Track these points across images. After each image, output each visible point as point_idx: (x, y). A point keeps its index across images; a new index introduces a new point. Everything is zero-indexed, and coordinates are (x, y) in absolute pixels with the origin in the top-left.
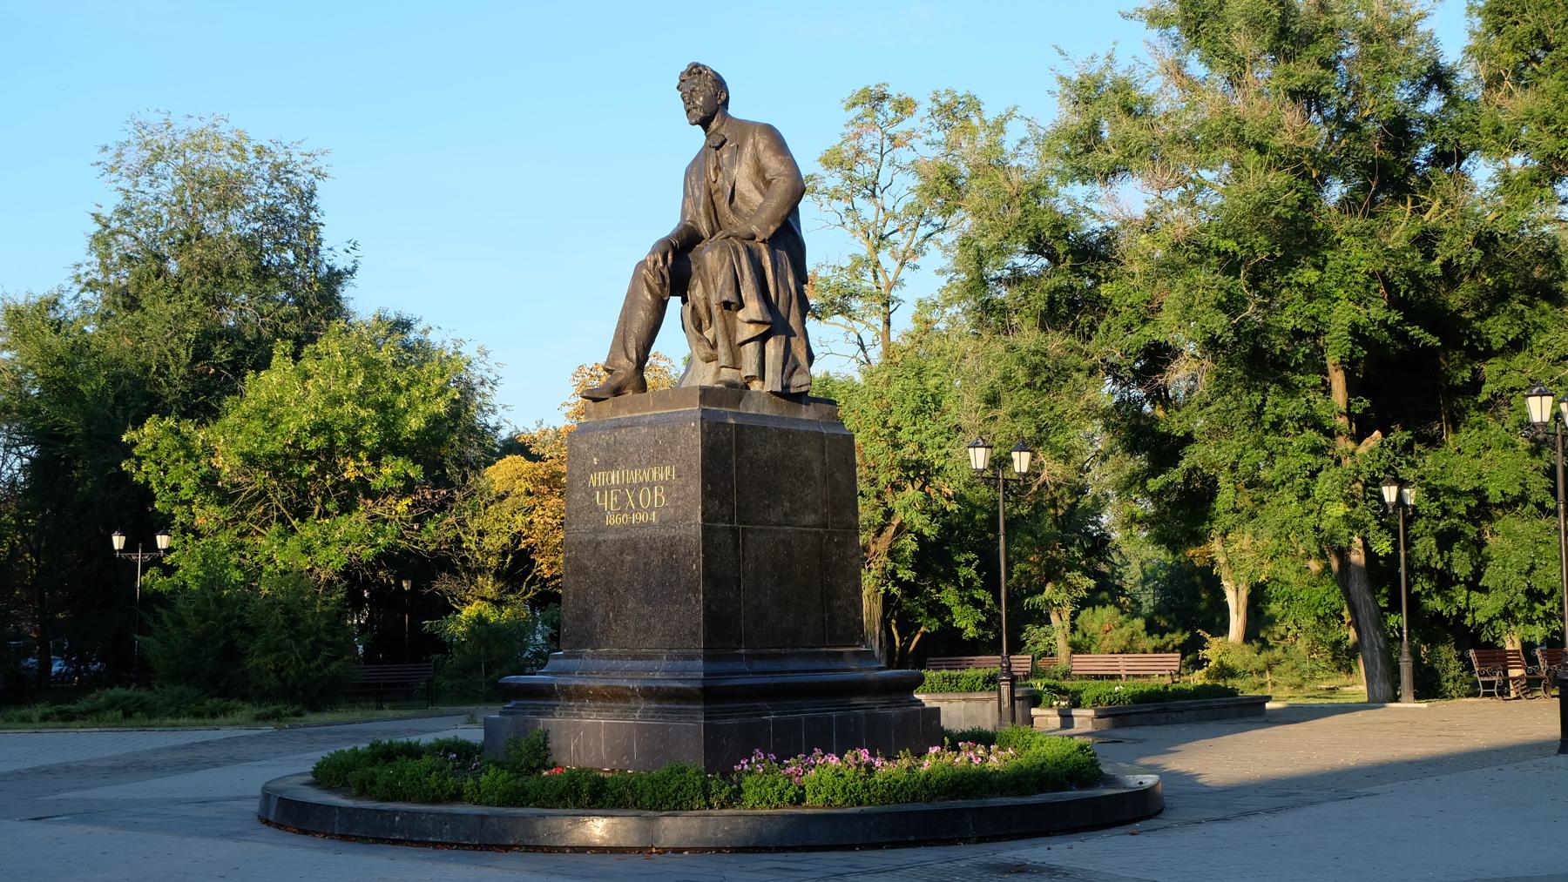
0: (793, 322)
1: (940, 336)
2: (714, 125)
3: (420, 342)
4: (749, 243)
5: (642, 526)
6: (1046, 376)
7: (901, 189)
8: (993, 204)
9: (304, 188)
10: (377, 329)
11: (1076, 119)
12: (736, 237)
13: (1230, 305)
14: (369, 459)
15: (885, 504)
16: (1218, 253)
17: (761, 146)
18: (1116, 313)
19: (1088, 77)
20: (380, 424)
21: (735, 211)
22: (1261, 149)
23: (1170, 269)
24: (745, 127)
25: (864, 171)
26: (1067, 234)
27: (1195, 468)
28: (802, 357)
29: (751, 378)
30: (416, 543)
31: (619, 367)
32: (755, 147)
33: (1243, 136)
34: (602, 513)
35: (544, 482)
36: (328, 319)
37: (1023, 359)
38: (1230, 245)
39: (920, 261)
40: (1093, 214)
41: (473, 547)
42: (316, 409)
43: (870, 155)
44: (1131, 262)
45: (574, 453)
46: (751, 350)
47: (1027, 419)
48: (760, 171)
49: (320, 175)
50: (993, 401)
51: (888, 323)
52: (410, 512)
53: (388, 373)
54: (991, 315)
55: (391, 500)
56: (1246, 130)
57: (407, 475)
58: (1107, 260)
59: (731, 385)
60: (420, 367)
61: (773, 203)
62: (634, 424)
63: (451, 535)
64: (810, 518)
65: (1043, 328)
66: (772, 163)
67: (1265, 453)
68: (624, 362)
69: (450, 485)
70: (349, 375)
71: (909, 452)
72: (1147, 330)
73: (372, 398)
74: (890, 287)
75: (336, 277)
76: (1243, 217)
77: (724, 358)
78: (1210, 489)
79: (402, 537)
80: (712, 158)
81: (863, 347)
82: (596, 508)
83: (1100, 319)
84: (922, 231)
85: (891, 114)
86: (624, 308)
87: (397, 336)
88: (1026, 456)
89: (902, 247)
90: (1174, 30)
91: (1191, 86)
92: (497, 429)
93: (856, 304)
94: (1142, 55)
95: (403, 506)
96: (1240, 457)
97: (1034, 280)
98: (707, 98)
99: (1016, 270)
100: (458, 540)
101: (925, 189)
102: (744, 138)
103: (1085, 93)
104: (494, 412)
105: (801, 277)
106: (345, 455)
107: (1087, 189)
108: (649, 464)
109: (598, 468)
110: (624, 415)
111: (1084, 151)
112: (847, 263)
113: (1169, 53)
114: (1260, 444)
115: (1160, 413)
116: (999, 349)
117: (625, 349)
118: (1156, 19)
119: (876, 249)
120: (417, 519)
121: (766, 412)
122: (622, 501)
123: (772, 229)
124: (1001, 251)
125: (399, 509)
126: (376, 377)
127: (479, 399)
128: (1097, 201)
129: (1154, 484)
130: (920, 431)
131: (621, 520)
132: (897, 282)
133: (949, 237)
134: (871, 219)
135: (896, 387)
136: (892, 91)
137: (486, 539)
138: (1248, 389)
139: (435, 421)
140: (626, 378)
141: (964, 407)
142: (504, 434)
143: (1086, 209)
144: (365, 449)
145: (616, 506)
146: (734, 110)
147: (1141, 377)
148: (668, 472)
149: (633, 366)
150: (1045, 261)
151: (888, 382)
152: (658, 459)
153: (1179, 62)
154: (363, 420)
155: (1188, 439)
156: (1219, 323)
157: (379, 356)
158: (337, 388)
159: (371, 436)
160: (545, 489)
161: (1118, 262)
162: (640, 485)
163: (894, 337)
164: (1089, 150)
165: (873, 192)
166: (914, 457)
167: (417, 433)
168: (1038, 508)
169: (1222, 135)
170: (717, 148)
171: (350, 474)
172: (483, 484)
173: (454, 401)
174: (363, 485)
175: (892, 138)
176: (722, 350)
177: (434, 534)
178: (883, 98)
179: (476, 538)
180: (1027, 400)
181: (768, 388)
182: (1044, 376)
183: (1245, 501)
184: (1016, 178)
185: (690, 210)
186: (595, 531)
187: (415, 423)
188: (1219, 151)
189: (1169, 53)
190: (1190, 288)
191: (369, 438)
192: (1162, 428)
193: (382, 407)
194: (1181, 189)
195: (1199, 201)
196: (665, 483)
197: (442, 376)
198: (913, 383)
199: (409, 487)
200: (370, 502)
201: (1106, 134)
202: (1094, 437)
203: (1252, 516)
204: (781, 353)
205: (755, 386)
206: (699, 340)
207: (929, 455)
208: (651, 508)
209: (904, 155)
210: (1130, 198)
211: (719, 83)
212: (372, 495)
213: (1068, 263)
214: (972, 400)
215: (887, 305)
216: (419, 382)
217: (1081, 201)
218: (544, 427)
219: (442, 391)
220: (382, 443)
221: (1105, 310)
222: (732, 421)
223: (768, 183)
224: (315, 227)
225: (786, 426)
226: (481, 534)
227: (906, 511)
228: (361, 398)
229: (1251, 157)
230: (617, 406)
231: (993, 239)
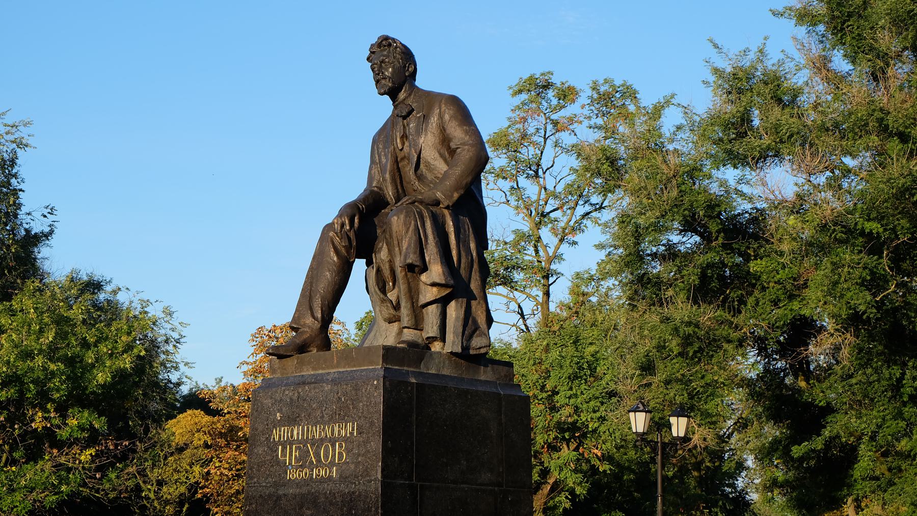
0: (474, 286)
1: (592, 309)
2: (402, 95)
3: (108, 301)
4: (434, 209)
5: (322, 481)
6: (699, 346)
7: (562, 168)
8: (651, 185)
9: (6, 156)
10: (70, 289)
11: (729, 108)
12: (421, 202)
13: (874, 283)
14: (56, 410)
15: (542, 463)
16: (862, 233)
17: (447, 117)
18: (764, 289)
19: (741, 69)
20: (68, 378)
21: (420, 178)
22: (904, 138)
23: (816, 248)
24: (431, 98)
25: (528, 152)
26: (720, 213)
27: (838, 436)
28: (481, 320)
29: (432, 339)
30: (97, 491)
31: (304, 325)
32: (441, 117)
33: (887, 126)
34: (283, 467)
35: (221, 435)
36: (24, 278)
37: (676, 329)
38: (873, 226)
39: (578, 237)
40: (742, 195)
41: (152, 496)
42: (8, 362)
43: (535, 138)
44: (780, 240)
45: (258, 409)
46: (432, 312)
47: (678, 386)
48: (445, 140)
49: (21, 144)
50: (648, 368)
51: (547, 294)
52: (93, 461)
53: (78, 329)
54: (645, 289)
55: (76, 449)
56: (890, 120)
57: (91, 425)
58: (756, 237)
59: (412, 345)
60: (109, 325)
61: (458, 171)
62: (318, 381)
63: (130, 483)
64: (486, 477)
65: (695, 302)
66: (457, 133)
67: (903, 424)
68: (309, 320)
69: (132, 436)
70: (41, 331)
71: (565, 414)
72: (795, 305)
73: (62, 352)
74: (550, 260)
75: (33, 240)
76: (886, 201)
77: (406, 320)
78: (850, 455)
79: (85, 485)
80: (399, 127)
81: (522, 315)
82: (278, 462)
83: (750, 294)
84: (581, 210)
85: (555, 102)
86: (311, 269)
87: (88, 296)
88: (683, 421)
89: (562, 224)
90: (821, 28)
91: (836, 81)
92: (178, 384)
93: (518, 276)
94: (788, 47)
95: (86, 456)
96: (879, 427)
97: (688, 256)
98: (394, 67)
99: (670, 246)
100: (138, 489)
101: (587, 169)
102: (430, 109)
103: (737, 83)
104: (176, 368)
105: (482, 243)
106: (34, 407)
107: (738, 172)
108: (332, 420)
109: (281, 423)
110: (308, 372)
111: (735, 138)
112: (510, 238)
113: (816, 50)
114: (899, 415)
115: (803, 384)
116: (655, 319)
117: (311, 309)
118: (804, 17)
119: (538, 225)
120: (99, 469)
121: (446, 372)
122: (304, 455)
123: (456, 196)
124: (659, 228)
125: (83, 458)
126: (67, 333)
127: (163, 356)
128: (748, 183)
129: (797, 451)
130: (576, 396)
131: (304, 474)
132: (557, 257)
133: (606, 216)
134: (534, 198)
135: (554, 354)
136: (556, 80)
137: (165, 489)
138: (889, 363)
139: (120, 376)
140: (308, 337)
141: (620, 372)
142: (185, 390)
143: (737, 191)
144: (53, 401)
145: (297, 460)
146: (423, 81)
147: (783, 350)
148: (349, 429)
149: (317, 325)
150: (697, 239)
151: (547, 349)
152: (340, 416)
153: (825, 58)
154: (53, 373)
155: (829, 409)
156: (862, 300)
157: (71, 314)
158: (29, 343)
159: (59, 389)
160: (222, 442)
161: (767, 241)
162: (322, 440)
163: (552, 307)
164: (741, 135)
165: (536, 172)
166: (570, 420)
167: (103, 386)
168: (683, 471)
169: (867, 125)
170: (404, 118)
171: (38, 424)
172: (164, 436)
173: (139, 357)
174: (49, 436)
175: (555, 123)
176: (405, 311)
177: (116, 482)
178: (547, 86)
179: (155, 487)
180: (677, 367)
181: (448, 349)
182: (696, 346)
183: (881, 469)
184: (673, 160)
185: (377, 177)
186: (276, 485)
187: (101, 377)
188: (864, 139)
189: (816, 50)
190: (836, 266)
191: (58, 390)
192: (806, 397)
193: (71, 362)
194: (828, 173)
195: (846, 185)
196: (346, 439)
197: (129, 334)
198: (571, 350)
199: (93, 438)
200: (55, 451)
201: (756, 122)
202: (736, 401)
203: (891, 483)
204: (462, 315)
205: (436, 347)
206: (383, 301)
207: (583, 417)
208: (332, 464)
209: (567, 139)
210: (781, 180)
211: (408, 56)
212: (59, 444)
213: (720, 240)
214: (629, 367)
215: (546, 277)
216: (107, 338)
217: (732, 183)
218: (223, 384)
219: (129, 348)
220: (70, 395)
221: (754, 286)
222: (414, 381)
223: (452, 152)
224: (15, 192)
225: (465, 387)
226: (160, 483)
227: (561, 470)
228: (52, 353)
229: (894, 146)
230: (301, 364)
231: (652, 215)
